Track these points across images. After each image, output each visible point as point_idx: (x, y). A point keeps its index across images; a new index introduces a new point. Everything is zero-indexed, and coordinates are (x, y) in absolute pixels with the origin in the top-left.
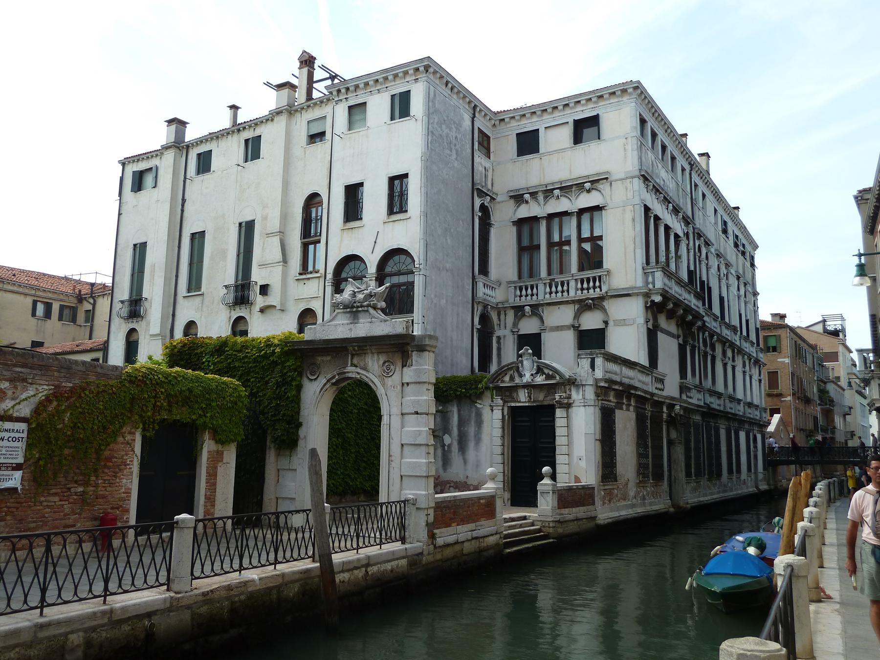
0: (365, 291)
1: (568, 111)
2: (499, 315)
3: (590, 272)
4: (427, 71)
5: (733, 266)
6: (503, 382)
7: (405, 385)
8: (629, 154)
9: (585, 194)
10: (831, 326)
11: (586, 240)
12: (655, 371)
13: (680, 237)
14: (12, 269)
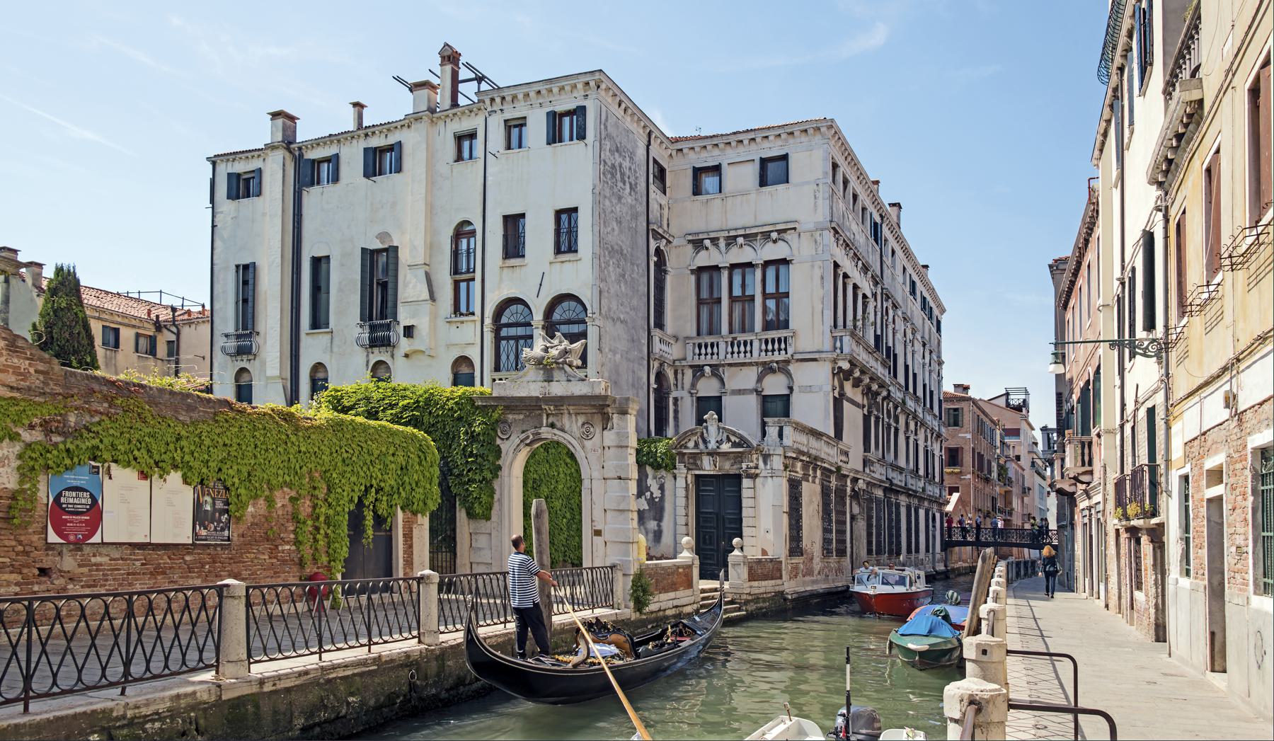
0: (559, 347)
2: (676, 373)
3: (774, 332)
4: (598, 87)
6: (686, 448)
7: (607, 449)
8: (820, 201)
9: (770, 244)
10: (1016, 399)
11: (771, 296)
12: (840, 442)
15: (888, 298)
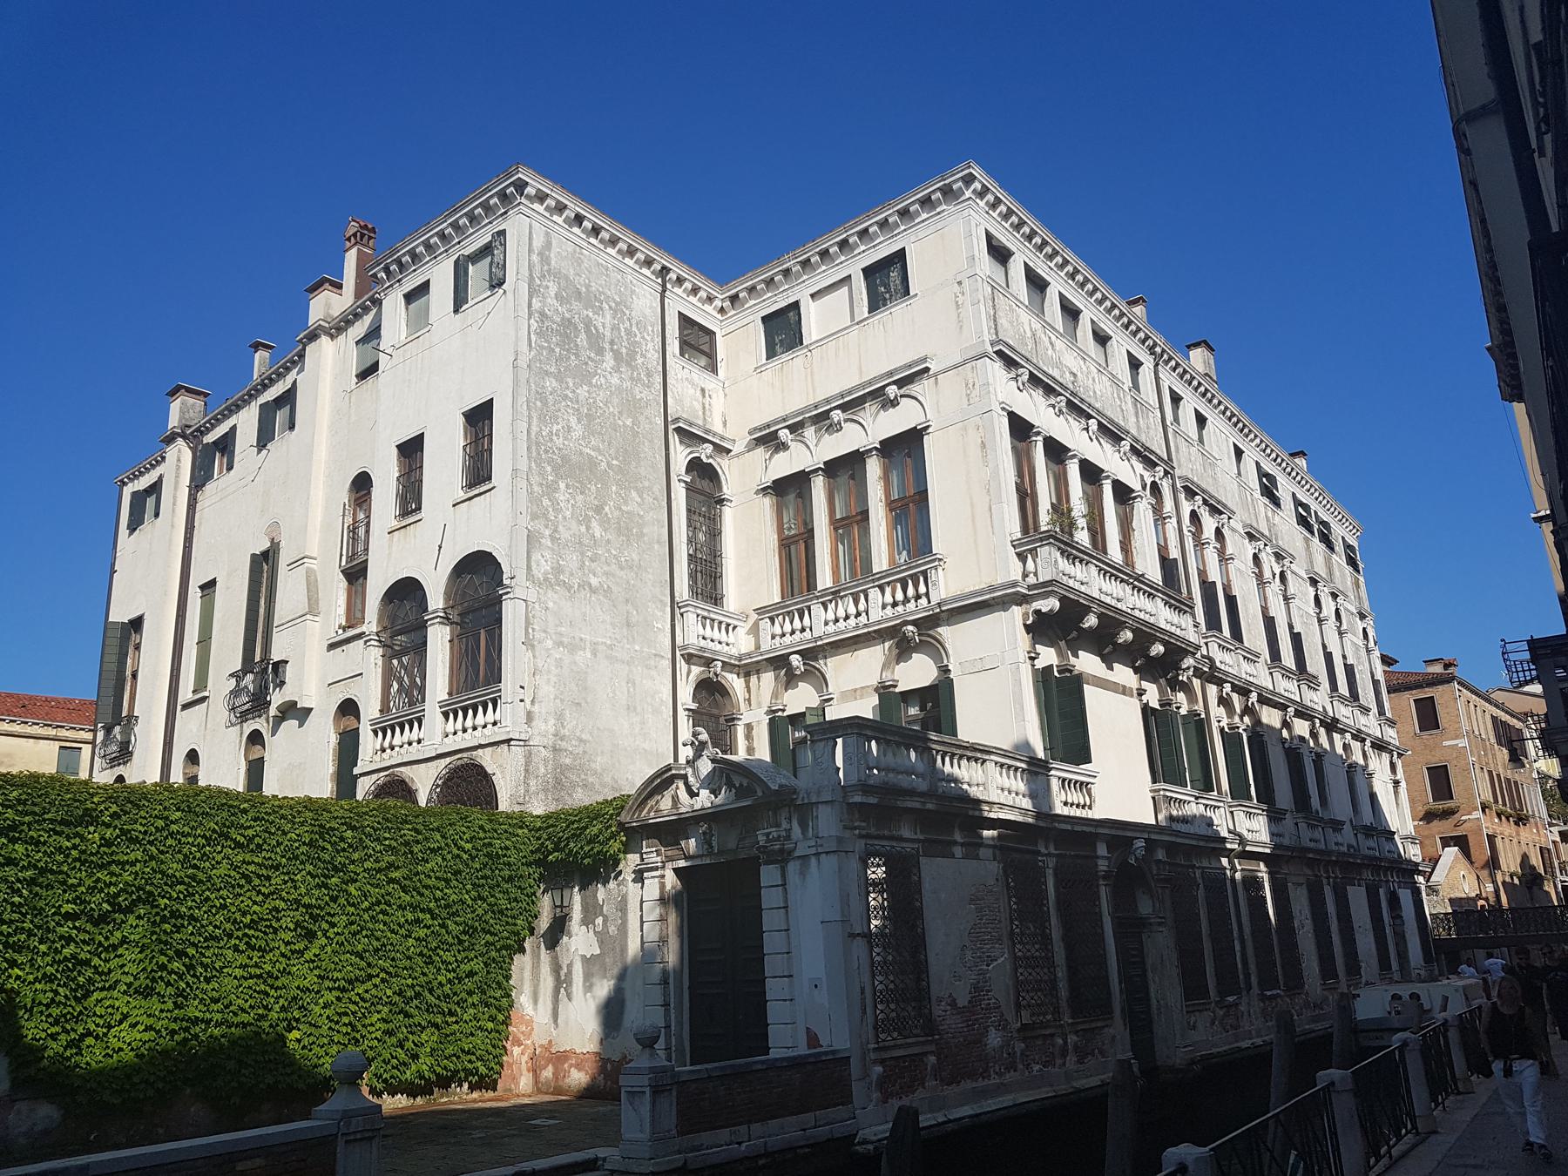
5: (1294, 558)
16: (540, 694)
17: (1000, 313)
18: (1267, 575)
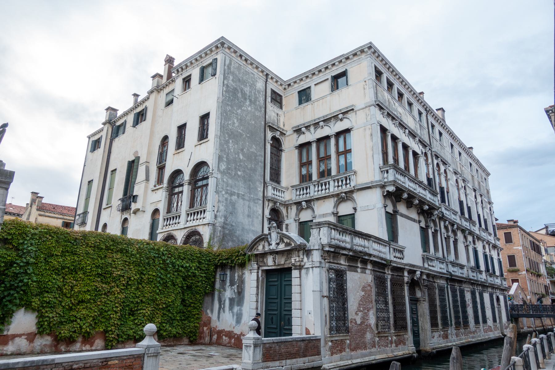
1: (328, 71)
5: (469, 182)
9: (339, 122)
13: (418, 154)
14: (52, 205)
15: (437, 157)
16: (220, 209)
17: (378, 92)
18: (460, 186)
